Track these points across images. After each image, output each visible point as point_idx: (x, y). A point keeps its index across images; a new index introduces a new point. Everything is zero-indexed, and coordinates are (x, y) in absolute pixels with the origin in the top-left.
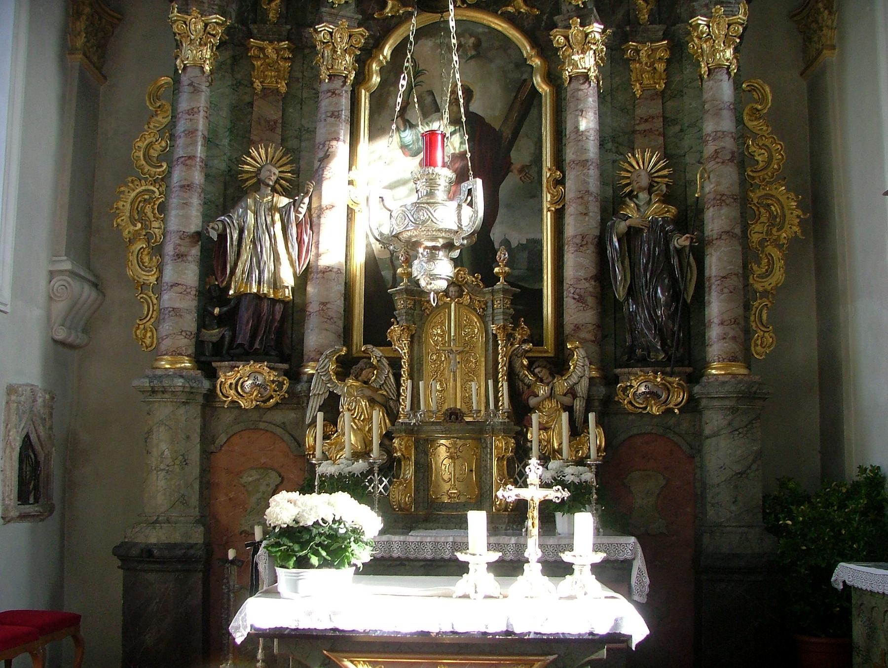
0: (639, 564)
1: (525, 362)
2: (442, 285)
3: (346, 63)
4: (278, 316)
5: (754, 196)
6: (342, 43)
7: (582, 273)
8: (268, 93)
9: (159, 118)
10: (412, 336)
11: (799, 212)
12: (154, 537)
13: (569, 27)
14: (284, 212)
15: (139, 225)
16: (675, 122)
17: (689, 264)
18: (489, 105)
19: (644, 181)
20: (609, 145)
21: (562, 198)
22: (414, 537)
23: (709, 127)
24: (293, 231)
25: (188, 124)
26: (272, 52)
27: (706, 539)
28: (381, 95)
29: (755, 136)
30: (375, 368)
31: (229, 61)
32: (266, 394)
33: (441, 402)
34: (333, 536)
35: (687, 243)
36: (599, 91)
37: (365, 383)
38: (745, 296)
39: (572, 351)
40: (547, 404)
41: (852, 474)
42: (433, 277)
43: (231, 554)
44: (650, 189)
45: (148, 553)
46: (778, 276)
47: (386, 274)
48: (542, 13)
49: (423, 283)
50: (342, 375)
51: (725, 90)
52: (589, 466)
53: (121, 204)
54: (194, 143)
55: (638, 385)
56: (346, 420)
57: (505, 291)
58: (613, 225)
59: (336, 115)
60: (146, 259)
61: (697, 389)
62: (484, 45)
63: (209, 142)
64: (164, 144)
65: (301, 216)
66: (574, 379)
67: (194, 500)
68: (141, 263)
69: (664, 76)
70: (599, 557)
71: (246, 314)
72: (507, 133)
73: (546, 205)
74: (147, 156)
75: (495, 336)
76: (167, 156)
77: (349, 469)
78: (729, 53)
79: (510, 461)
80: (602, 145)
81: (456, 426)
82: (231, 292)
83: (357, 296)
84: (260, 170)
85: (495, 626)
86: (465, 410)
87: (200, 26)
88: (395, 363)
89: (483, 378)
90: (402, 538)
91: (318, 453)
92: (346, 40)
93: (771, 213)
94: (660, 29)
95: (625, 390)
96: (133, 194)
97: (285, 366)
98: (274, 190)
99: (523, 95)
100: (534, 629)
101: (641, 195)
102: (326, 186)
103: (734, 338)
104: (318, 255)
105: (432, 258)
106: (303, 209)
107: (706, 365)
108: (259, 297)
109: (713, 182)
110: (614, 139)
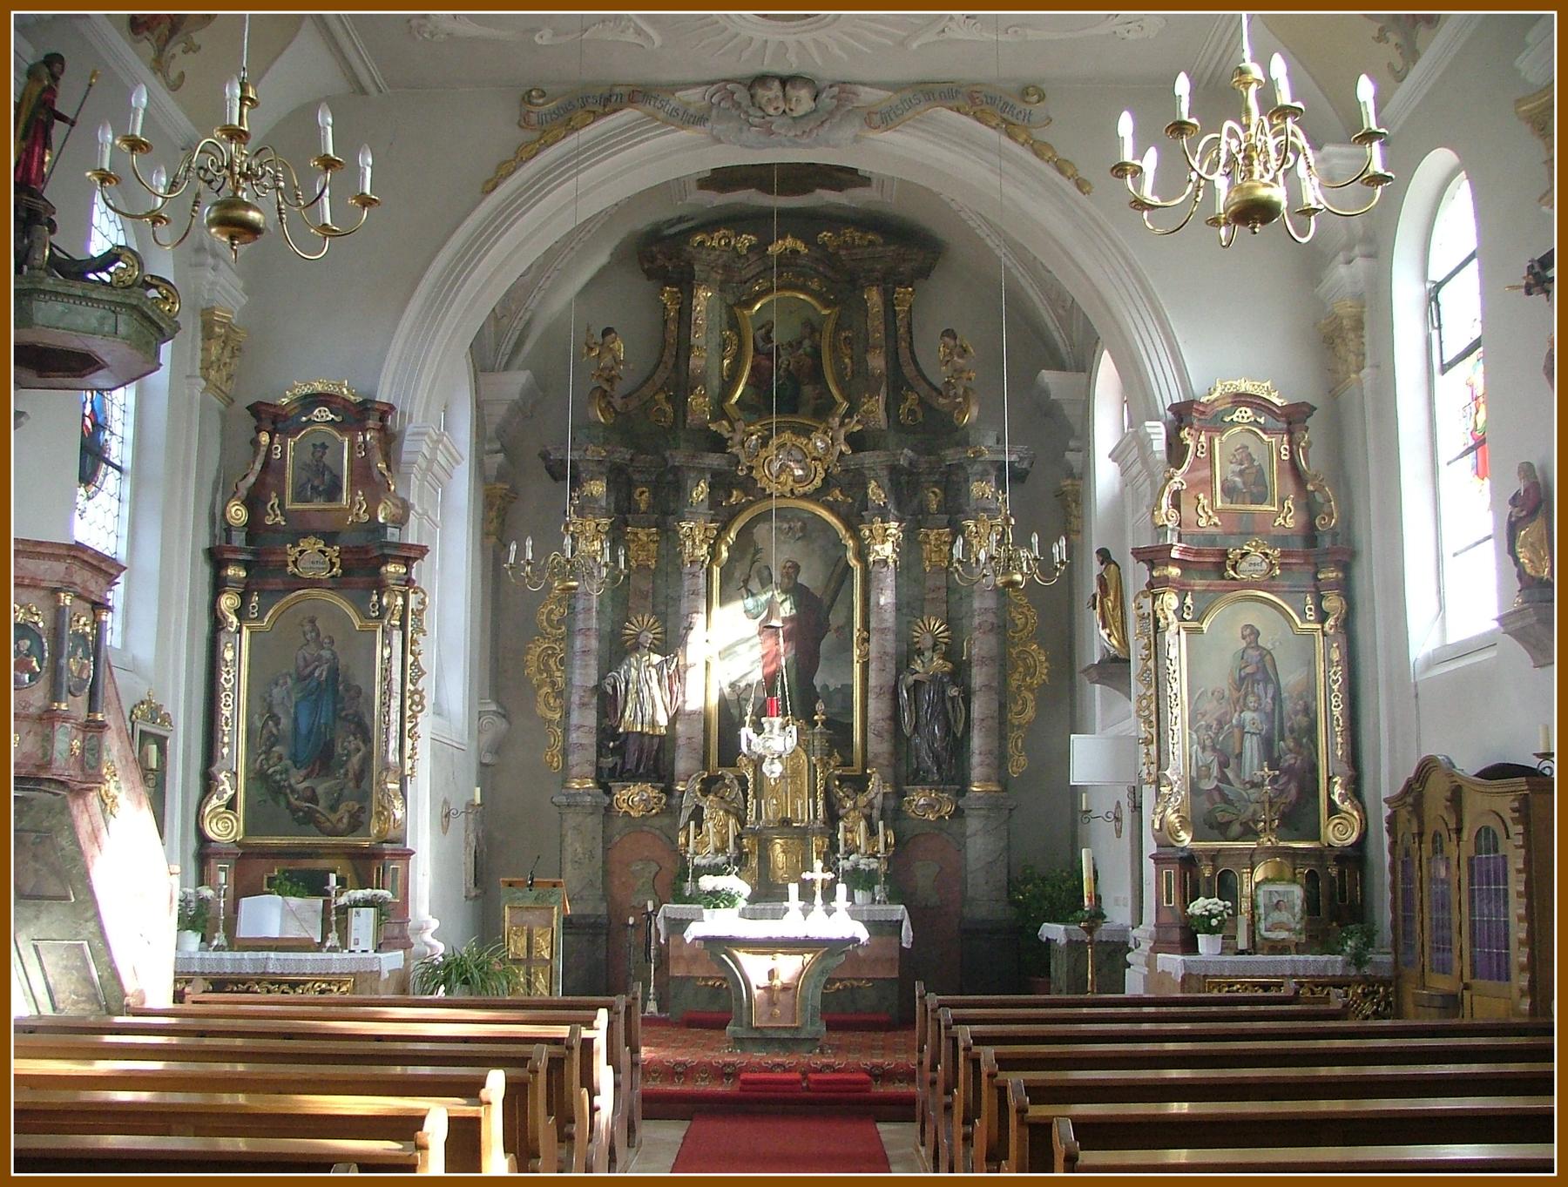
0: (906, 924)
2: (777, 775)
5: (1014, 652)
7: (879, 715)
14: (659, 668)
19: (929, 642)
23: (976, 605)
24: (666, 682)
33: (775, 815)
38: (1001, 726)
43: (631, 920)
44: (934, 648)
46: (1030, 713)
47: (735, 712)
55: (919, 798)
56: (709, 825)
59: (695, 593)
67: (599, 883)
68: (547, 704)
71: (632, 748)
72: (827, 601)
74: (549, 620)
79: (826, 854)
85: (801, 934)
88: (743, 781)
91: (691, 849)
93: (1025, 664)
98: (650, 649)
99: (839, 570)
105: (772, 763)
107: (970, 784)
108: (641, 734)
109: (979, 646)
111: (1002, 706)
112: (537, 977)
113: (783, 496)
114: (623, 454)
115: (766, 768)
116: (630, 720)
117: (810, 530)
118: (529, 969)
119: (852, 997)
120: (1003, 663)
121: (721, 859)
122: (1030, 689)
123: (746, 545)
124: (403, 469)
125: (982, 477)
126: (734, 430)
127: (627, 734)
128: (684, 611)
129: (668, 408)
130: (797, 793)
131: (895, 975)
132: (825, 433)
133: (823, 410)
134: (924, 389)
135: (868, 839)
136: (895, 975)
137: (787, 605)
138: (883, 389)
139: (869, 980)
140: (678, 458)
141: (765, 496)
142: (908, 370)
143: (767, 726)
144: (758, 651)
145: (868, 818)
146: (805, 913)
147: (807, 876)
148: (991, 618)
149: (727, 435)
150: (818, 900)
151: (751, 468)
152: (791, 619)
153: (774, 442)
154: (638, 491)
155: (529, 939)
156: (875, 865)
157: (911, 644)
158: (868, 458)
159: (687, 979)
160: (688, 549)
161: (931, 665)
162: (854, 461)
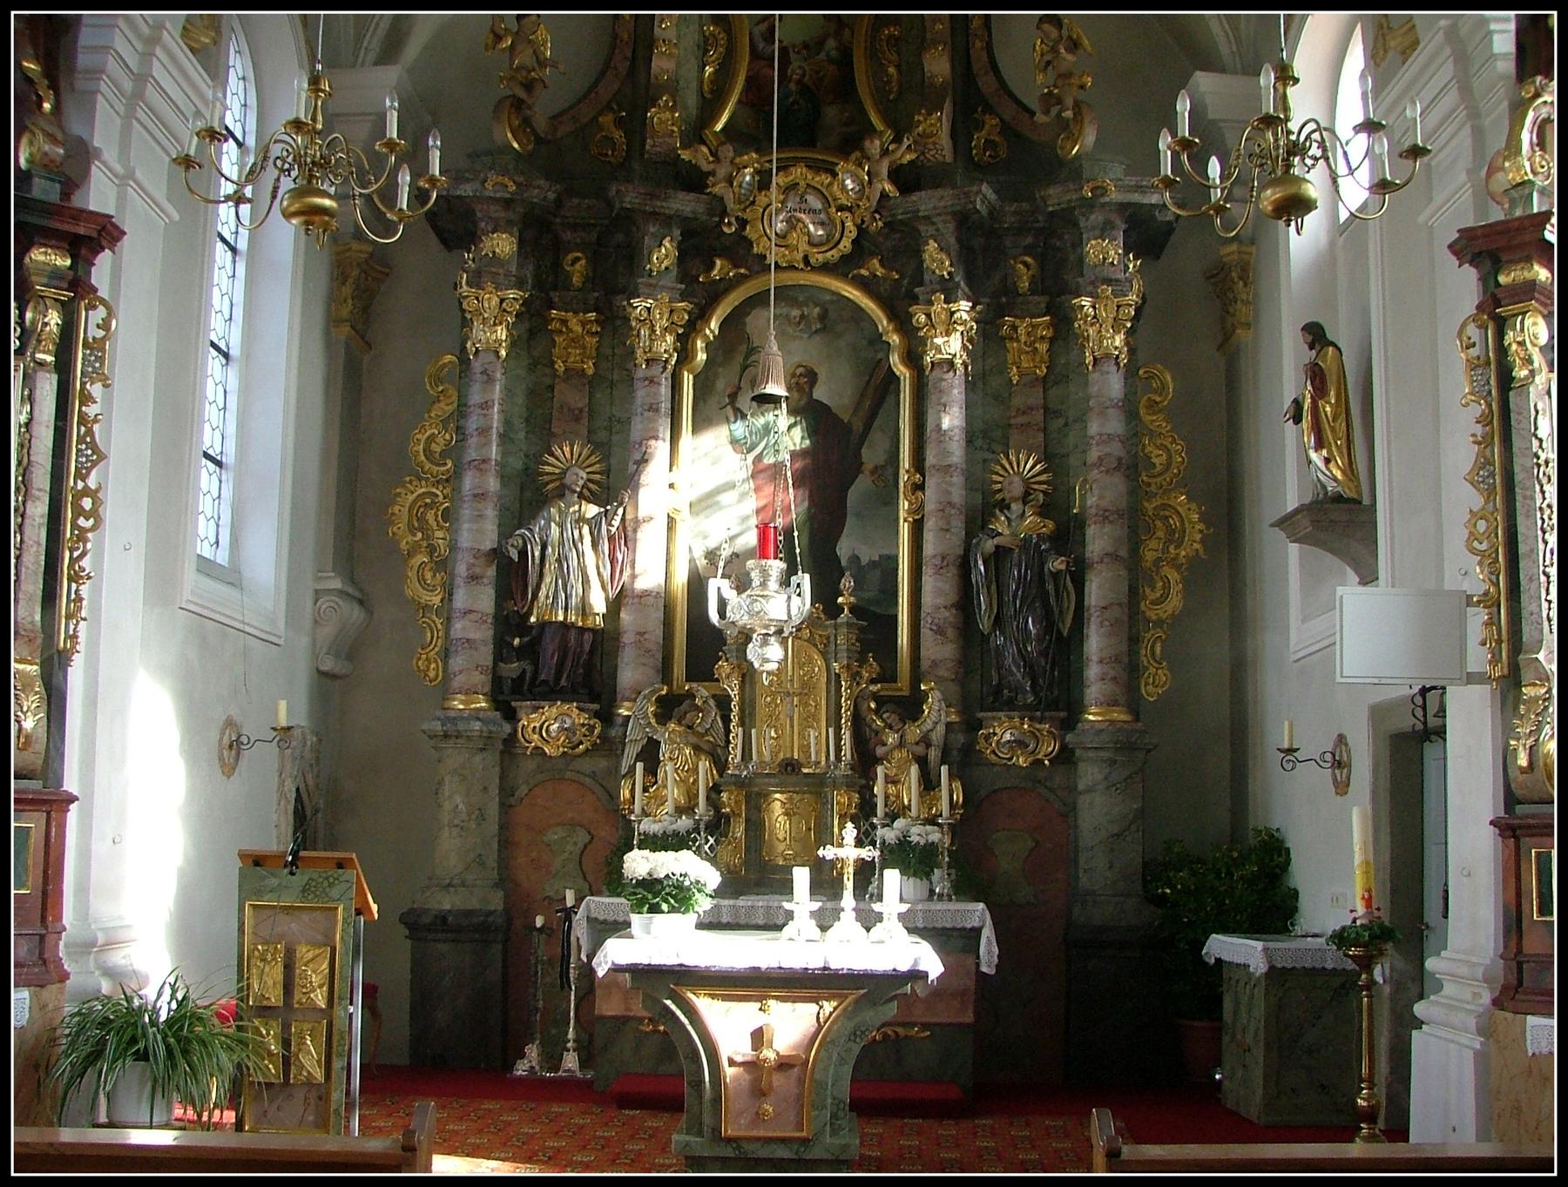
0: (988, 933)
1: (873, 705)
3: (666, 345)
4: (587, 647)
5: (1150, 506)
6: (661, 322)
7: (940, 601)
8: (573, 374)
9: (442, 405)
10: (744, 676)
11: (1201, 526)
12: (446, 902)
13: (931, 303)
14: (594, 524)
15: (420, 535)
16: (1057, 414)
17: (1065, 587)
18: (832, 391)
19: (1017, 489)
20: (979, 443)
21: (922, 506)
22: (742, 902)
23: (1094, 428)
25: (482, 421)
26: (575, 326)
27: (1077, 910)
28: (707, 378)
29: (1151, 434)
30: (699, 709)
31: (525, 336)
32: (575, 740)
33: (774, 754)
34: (679, 887)
35: (1063, 567)
36: (967, 381)
37: (689, 727)
38: (1132, 622)
39: (926, 693)
40: (897, 754)
41: (1252, 841)
42: (767, 661)
44: (1025, 498)
45: (442, 920)
46: (1174, 603)
48: (902, 277)
49: (756, 665)
50: (663, 717)
51: (1113, 384)
52: (939, 825)
53: (397, 508)
54: (488, 444)
55: (1003, 731)
56: (667, 770)
57: (849, 625)
58: (978, 544)
59: (654, 408)
60: (428, 575)
61: (1069, 737)
62: (832, 315)
63: (504, 438)
64: (448, 437)
65: (613, 530)
66: (929, 725)
67: (492, 861)
68: (421, 579)
69: (1046, 358)
70: (904, 907)
71: (550, 647)
72: (858, 426)
73: (902, 515)
74: (428, 452)
75: (838, 676)
76: (454, 451)
77: (674, 827)
78: (1119, 340)
80: (970, 441)
81: (793, 779)
82: (533, 619)
83: (678, 623)
84: (564, 472)
86: (803, 760)
87: (495, 301)
88: (723, 702)
89: (824, 724)
90: (732, 902)
91: (637, 807)
92: (666, 316)
94: (1042, 301)
95: (987, 737)
96: (411, 498)
97: (596, 706)
98: (581, 496)
100: (846, 966)
101: (1014, 506)
102: (643, 494)
103: (1114, 679)
104: (633, 577)
105: (765, 643)
106: (616, 522)
108: (565, 626)
109: (1097, 493)
110: (985, 434)
111: (1134, 593)
112: (302, 1043)
113: (792, 268)
114: (543, 192)
115: (752, 652)
116: (549, 605)
117: (832, 319)
118: (286, 1027)
119: (894, 1062)
120: (1135, 522)
121: (684, 823)
122: (1174, 563)
123: (736, 346)
124: (80, 84)
125: (1104, 231)
126: (718, 160)
127: (543, 625)
128: (635, 435)
129: (618, 135)
130: (809, 720)
131: (969, 1017)
132: (860, 165)
133: (851, 144)
134: (1008, 111)
135: (921, 796)
136: (969, 1017)
137: (797, 433)
138: (948, 106)
139: (925, 1026)
140: (630, 197)
141: (760, 265)
142: (986, 83)
143: (755, 575)
144: (752, 503)
145: (922, 762)
146: (825, 922)
147: (828, 852)
148: (1116, 449)
149: (705, 167)
150: (848, 900)
151: (743, 223)
152: (803, 453)
153: (778, 180)
154: (570, 257)
155: (289, 968)
156: (935, 836)
157: (987, 493)
158: (926, 201)
159: (622, 1021)
160: (644, 340)
161: (1019, 525)
162: (904, 206)
